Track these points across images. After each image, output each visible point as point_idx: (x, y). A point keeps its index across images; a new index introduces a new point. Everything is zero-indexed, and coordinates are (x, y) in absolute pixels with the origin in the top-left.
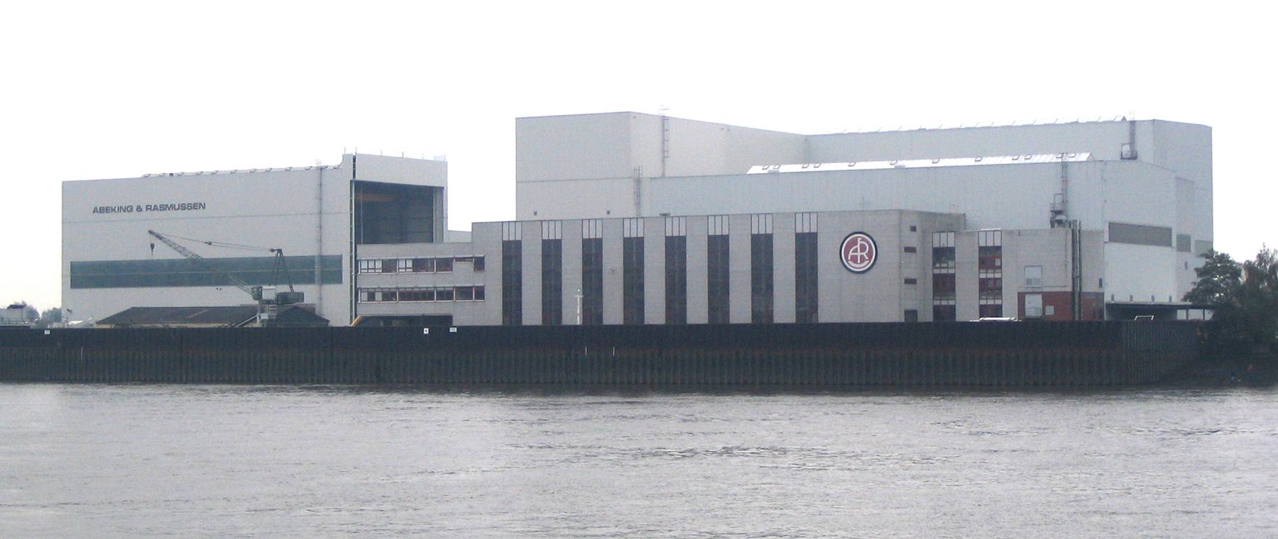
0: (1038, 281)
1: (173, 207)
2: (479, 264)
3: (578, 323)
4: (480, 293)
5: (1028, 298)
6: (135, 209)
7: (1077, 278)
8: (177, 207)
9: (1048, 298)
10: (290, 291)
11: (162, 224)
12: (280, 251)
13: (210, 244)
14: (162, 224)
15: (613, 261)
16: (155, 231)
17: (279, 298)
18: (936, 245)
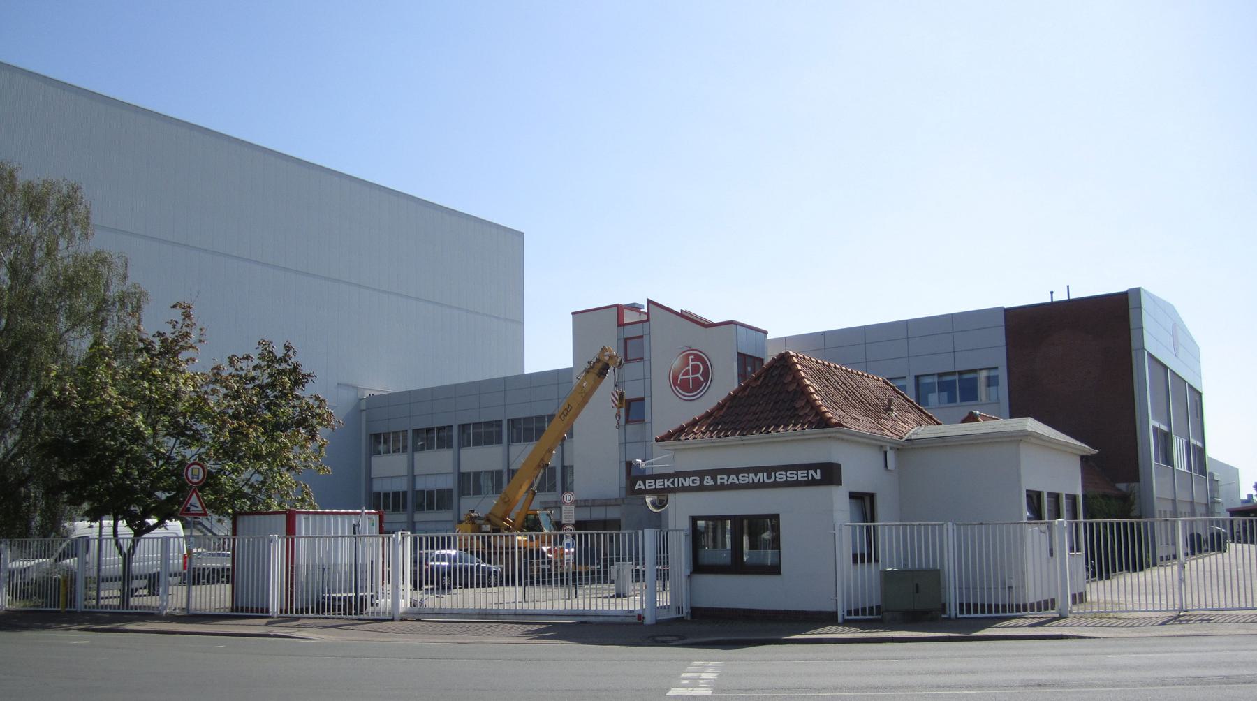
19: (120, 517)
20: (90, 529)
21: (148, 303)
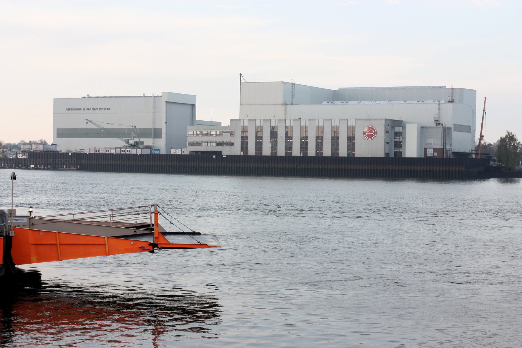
0: (431, 144)
1: (97, 109)
2: (232, 134)
3: (270, 155)
4: (232, 144)
5: (428, 150)
6: (82, 109)
7: (445, 144)
8: (99, 109)
9: (435, 150)
10: (139, 141)
11: (91, 116)
12: (135, 126)
13: (109, 124)
14: (91, 116)
15: (281, 135)
16: (88, 119)
17: (135, 143)
18: (396, 131)
19: (471, 157)
20: (451, 104)
21: (421, 262)
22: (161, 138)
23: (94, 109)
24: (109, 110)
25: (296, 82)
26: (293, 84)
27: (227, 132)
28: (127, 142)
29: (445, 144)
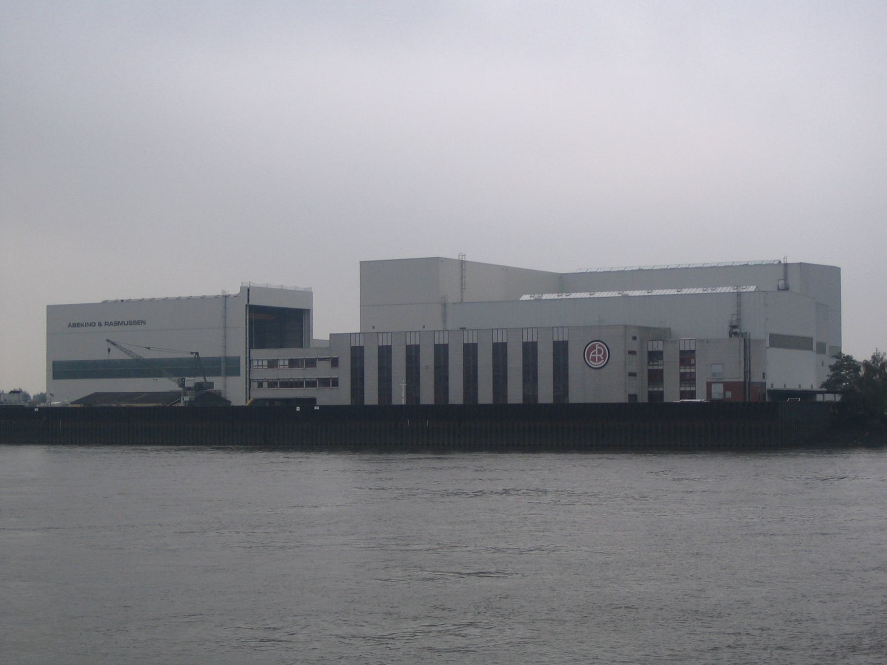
1: (123, 323)
2: (335, 362)
3: (403, 404)
4: (335, 383)
6: (97, 324)
7: (747, 372)
8: (126, 323)
9: (728, 386)
10: (204, 381)
12: (197, 353)
13: (149, 348)
15: (427, 360)
18: (650, 349)
22: (238, 374)
23: (117, 324)
24: (145, 324)
25: (468, 258)
26: (462, 262)
27: (324, 359)
28: (182, 385)
29: (747, 372)
